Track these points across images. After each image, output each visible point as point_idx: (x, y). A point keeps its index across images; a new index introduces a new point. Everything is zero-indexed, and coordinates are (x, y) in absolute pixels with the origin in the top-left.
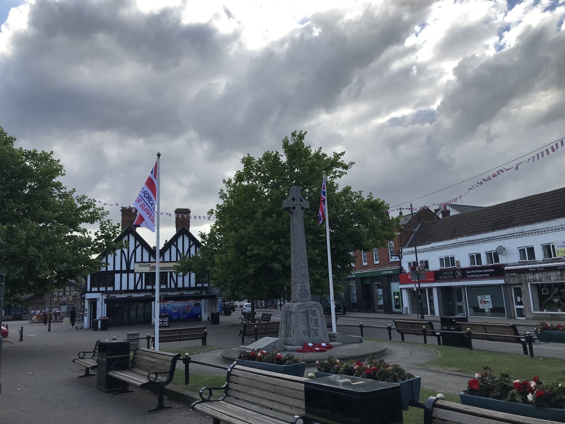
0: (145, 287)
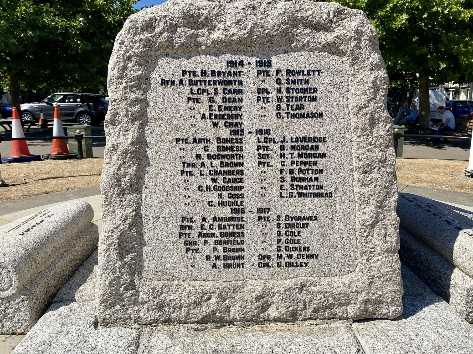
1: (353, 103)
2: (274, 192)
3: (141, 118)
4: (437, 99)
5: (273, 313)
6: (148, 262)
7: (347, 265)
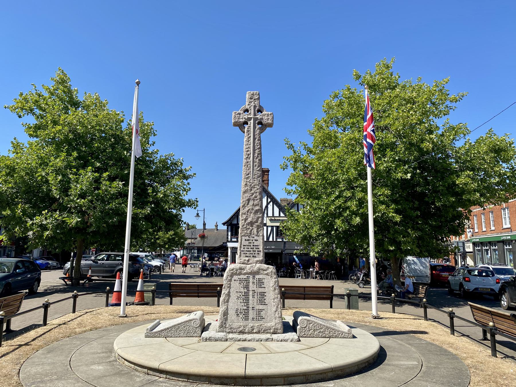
0: (276, 239)
1: (271, 285)
2: (255, 304)
3: (230, 287)
4: (421, 265)
5: (255, 331)
6: (229, 318)
7: (271, 321)
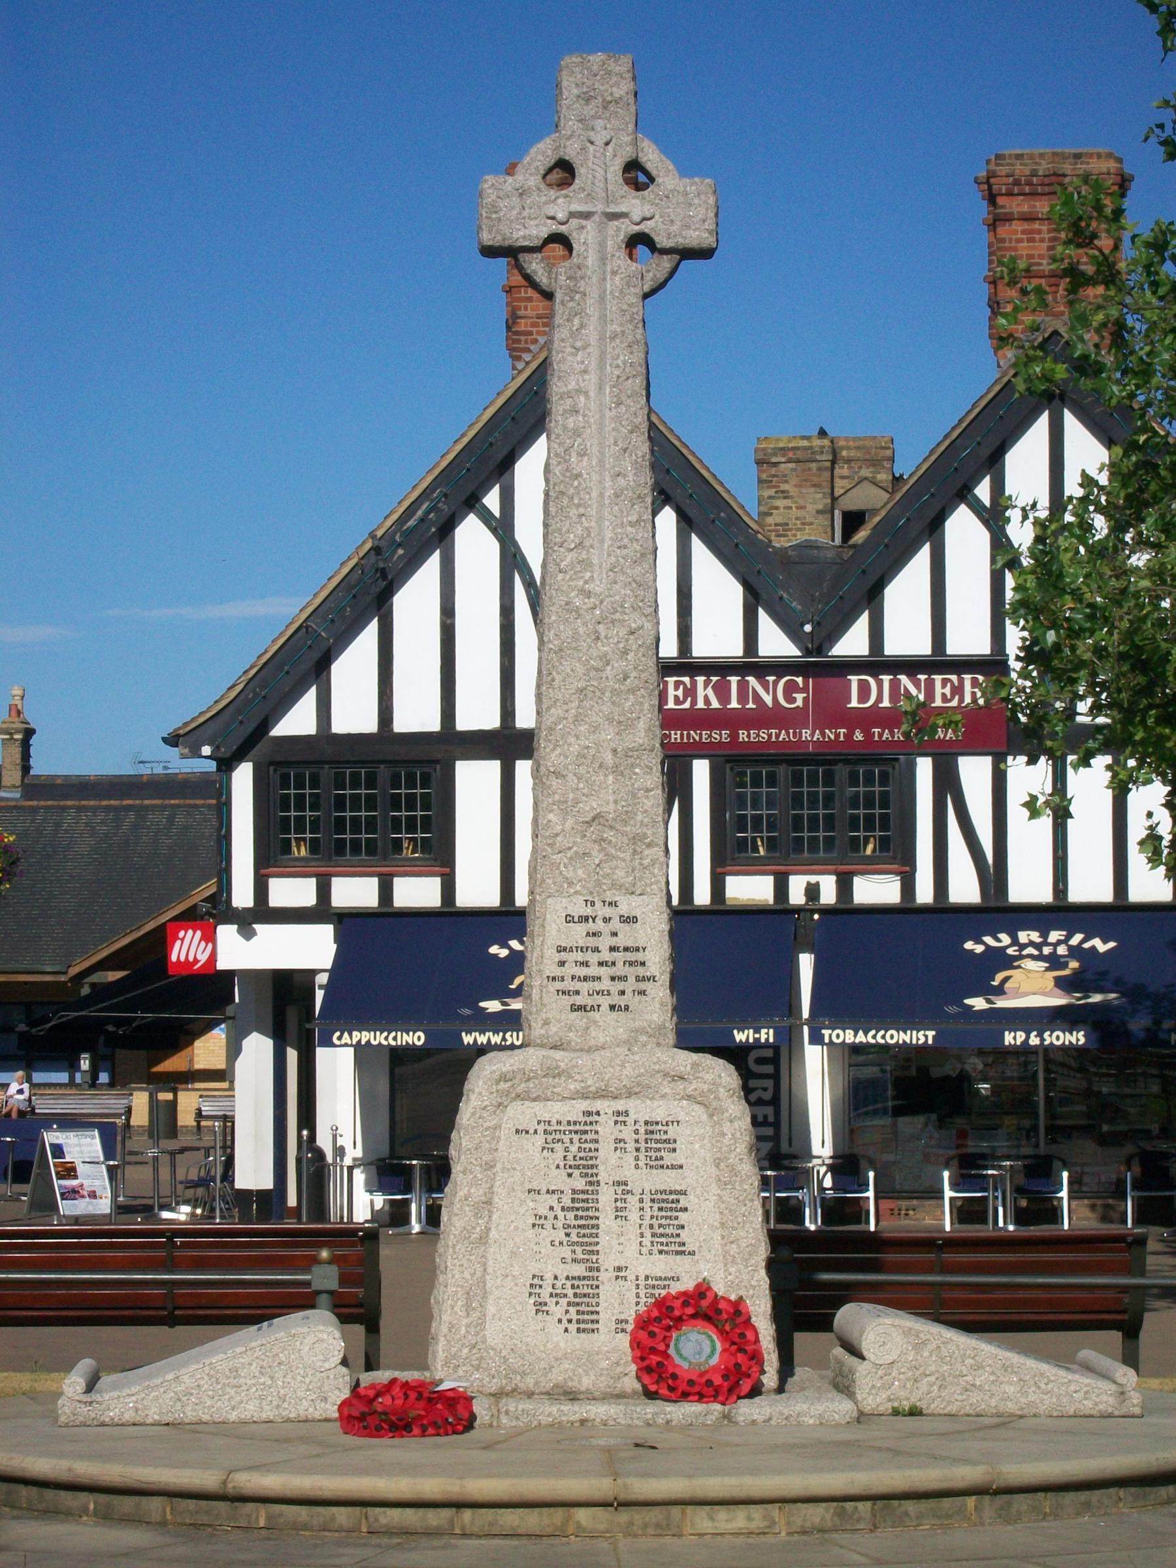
0: (261, 891)
